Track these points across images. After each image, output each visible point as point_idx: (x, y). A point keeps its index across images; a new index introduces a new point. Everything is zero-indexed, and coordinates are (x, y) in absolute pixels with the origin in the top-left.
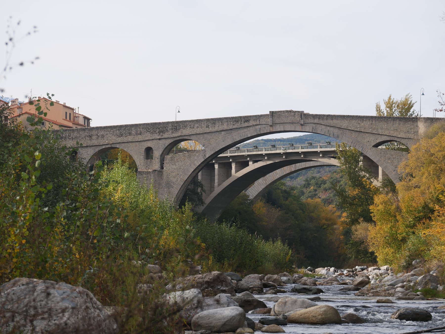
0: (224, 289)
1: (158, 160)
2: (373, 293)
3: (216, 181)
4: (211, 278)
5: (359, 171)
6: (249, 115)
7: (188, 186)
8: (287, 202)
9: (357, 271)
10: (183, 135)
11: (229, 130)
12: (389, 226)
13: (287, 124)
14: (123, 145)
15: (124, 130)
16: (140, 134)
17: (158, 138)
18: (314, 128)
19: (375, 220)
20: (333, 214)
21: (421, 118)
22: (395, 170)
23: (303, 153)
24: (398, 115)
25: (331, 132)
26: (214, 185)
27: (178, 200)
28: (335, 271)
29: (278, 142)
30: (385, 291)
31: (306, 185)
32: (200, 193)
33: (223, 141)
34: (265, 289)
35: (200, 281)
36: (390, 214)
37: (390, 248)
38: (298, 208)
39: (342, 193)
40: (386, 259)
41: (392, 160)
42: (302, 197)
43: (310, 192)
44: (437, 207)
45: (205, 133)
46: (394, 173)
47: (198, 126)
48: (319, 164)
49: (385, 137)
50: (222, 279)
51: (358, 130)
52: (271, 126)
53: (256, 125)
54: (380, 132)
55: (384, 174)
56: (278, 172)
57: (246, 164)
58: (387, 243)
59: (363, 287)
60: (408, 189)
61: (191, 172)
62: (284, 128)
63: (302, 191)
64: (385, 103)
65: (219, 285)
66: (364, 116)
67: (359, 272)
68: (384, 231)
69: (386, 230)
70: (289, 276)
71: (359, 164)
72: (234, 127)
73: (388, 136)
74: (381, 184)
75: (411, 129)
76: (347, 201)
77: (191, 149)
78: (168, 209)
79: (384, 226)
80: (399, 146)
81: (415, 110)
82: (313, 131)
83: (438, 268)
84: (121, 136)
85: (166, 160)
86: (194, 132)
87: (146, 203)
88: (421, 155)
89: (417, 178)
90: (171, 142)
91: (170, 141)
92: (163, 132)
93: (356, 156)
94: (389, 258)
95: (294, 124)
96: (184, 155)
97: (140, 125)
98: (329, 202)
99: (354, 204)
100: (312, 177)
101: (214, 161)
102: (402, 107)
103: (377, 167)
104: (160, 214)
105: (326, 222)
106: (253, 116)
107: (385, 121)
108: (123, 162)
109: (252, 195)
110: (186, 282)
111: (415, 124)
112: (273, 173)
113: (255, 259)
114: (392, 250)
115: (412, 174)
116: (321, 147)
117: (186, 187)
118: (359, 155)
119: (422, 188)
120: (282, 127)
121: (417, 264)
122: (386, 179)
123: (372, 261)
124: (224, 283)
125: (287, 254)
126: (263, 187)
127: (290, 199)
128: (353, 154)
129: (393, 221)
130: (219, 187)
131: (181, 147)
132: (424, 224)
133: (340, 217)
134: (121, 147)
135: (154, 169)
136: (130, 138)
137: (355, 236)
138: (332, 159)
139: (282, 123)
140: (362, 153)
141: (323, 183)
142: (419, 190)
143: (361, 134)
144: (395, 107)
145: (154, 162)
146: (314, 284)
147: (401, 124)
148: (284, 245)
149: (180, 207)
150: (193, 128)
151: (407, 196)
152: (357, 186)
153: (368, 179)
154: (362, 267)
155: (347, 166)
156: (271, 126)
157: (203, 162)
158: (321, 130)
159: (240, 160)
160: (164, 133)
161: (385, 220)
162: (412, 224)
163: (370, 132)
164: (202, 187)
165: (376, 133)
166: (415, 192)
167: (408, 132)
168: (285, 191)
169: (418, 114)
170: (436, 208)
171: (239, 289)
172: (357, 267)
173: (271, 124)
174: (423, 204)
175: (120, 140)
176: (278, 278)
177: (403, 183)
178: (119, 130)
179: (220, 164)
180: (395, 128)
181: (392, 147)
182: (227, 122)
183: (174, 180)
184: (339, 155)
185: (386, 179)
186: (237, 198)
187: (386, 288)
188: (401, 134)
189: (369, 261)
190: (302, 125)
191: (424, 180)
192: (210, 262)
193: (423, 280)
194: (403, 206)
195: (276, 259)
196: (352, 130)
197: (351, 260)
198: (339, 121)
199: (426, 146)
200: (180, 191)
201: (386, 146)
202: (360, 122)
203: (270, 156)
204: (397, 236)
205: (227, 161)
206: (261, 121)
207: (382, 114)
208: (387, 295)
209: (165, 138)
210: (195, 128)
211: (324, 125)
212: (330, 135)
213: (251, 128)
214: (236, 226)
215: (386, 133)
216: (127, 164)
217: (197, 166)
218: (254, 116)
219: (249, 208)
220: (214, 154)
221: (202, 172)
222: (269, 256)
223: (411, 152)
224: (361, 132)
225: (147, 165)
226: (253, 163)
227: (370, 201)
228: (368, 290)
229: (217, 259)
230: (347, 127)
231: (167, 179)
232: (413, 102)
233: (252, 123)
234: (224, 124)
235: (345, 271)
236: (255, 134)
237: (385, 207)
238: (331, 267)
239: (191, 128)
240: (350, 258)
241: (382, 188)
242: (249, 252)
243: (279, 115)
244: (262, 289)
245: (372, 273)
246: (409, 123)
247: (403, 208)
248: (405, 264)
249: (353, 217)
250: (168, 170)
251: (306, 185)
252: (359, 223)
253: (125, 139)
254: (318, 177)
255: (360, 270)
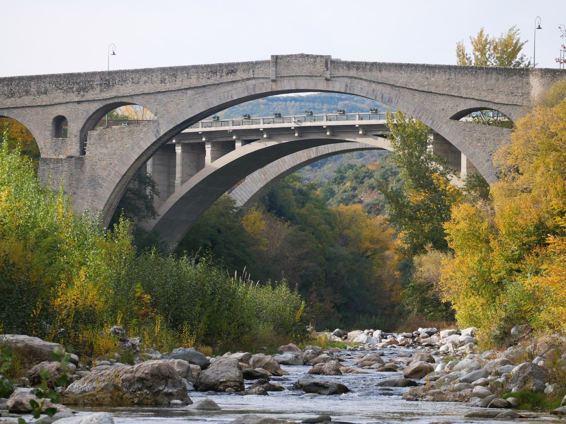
0: (170, 391)
1: (76, 138)
2: (433, 394)
3: (178, 175)
4: (146, 372)
5: (426, 161)
6: (235, 62)
7: (128, 184)
8: (303, 211)
9: (421, 336)
10: (119, 95)
11: (201, 87)
12: (477, 259)
13: (301, 78)
14: (15, 111)
15: (17, 85)
16: (45, 93)
17: (77, 100)
18: (349, 85)
19: (452, 247)
20: (384, 231)
21: (536, 70)
22: (488, 160)
23: (329, 127)
24: (495, 64)
25: (379, 93)
26: (174, 183)
27: (111, 209)
28: (383, 337)
29: (291, 101)
30: (454, 391)
31: (338, 179)
32: (150, 197)
33: (190, 107)
34: (249, 381)
35: (128, 378)
36: (478, 237)
37: (477, 297)
38: (321, 220)
39: (397, 198)
40: (470, 316)
41: (485, 141)
42: (330, 201)
43: (345, 191)
44: (551, 239)
45: (159, 92)
46: (487, 164)
47: (147, 79)
48: (358, 146)
49: (473, 101)
50: (167, 375)
51: (426, 89)
52: (274, 81)
53: (248, 79)
54: (464, 93)
55: (470, 166)
56: (287, 160)
57: (230, 146)
58: (472, 287)
59: (421, 378)
60: (511, 193)
61: (134, 160)
62: (296, 84)
63: (331, 189)
64: (472, 43)
65: (162, 384)
66: (436, 65)
67: (424, 338)
68: (468, 267)
69: (471, 264)
70: (297, 350)
71: (427, 148)
72: (209, 82)
73: (477, 100)
74: (465, 183)
75: (517, 88)
76: (405, 212)
77: (136, 118)
78: (88, 230)
79: (469, 259)
80: (496, 118)
81: (525, 56)
82: (346, 90)
83: (549, 349)
84: (12, 97)
85: (90, 139)
86: (140, 90)
87: (49, 220)
88: (533, 136)
89: (526, 175)
90: (98, 108)
91: (98, 106)
92: (85, 89)
93: (422, 135)
94: (476, 314)
95: (314, 78)
96: (122, 130)
97: (45, 77)
98: (378, 209)
99: (417, 219)
100: (349, 164)
101: (174, 141)
102: (502, 50)
103: (458, 154)
104: (74, 238)
105: (372, 246)
106: (243, 64)
107: (472, 74)
108: (11, 147)
109: (240, 199)
110: (104, 378)
111: (525, 80)
112: (279, 162)
113: (237, 321)
114: (482, 301)
115: (517, 168)
116: (361, 118)
117: (124, 187)
118: (426, 133)
119: (535, 193)
120: (292, 82)
121: (520, 332)
122: (473, 176)
123: (446, 317)
124: (170, 380)
125: (297, 308)
126: (261, 185)
127: (309, 205)
128: (417, 130)
129: (483, 249)
130: (183, 186)
131: (118, 114)
132: (537, 255)
133: (395, 236)
134: (13, 114)
135: (69, 154)
136: (27, 100)
137: (418, 274)
138: (380, 138)
139: (293, 76)
140: (432, 129)
141: (368, 176)
142: (529, 197)
143: (431, 97)
144: (489, 50)
145: (69, 142)
146: (336, 370)
147: (500, 79)
148: (292, 291)
149: (111, 227)
150: (138, 83)
151: (508, 207)
152: (422, 186)
153: (442, 174)
154: (429, 329)
155: (406, 151)
156: (274, 81)
157: (155, 143)
158: (362, 89)
159: (220, 140)
160: (87, 92)
161: (470, 248)
162: (516, 255)
163: (446, 93)
164: (153, 187)
165: (456, 94)
166: (522, 201)
167: (512, 93)
168: (300, 191)
169: (529, 63)
170: (549, 240)
171: (201, 383)
172: (420, 330)
173: (274, 77)
174: (535, 221)
175: (9, 102)
176: (272, 361)
177: (501, 183)
178: (8, 85)
179: (184, 146)
180: (490, 87)
181: (485, 119)
182: (197, 73)
183: (104, 174)
184: (392, 133)
185: (473, 176)
186: (215, 204)
187: (456, 385)
188: (500, 97)
189: (443, 317)
190: (327, 80)
191: (538, 179)
192: (157, 329)
193: (521, 374)
194: (500, 223)
195: (279, 317)
196: (415, 90)
197: (411, 315)
198: (392, 74)
199: (542, 119)
200: (114, 194)
201: (474, 117)
202: (428, 75)
203: (272, 133)
204: (490, 275)
205: (198, 141)
206: (256, 72)
207: (467, 61)
208: (457, 399)
209: (88, 101)
210: (141, 83)
211: (366, 80)
212: (376, 97)
213: (239, 85)
214: (206, 262)
215: (475, 95)
216: (18, 150)
217: (143, 150)
218: (244, 63)
219: (235, 222)
220: (174, 128)
221: (154, 160)
222: (266, 312)
223: (516, 131)
224: (431, 92)
225: (56, 147)
226: (242, 145)
227: (445, 213)
228: (424, 390)
229: (171, 322)
230: (406, 84)
231: (92, 172)
232: (521, 42)
233: (240, 75)
234: (192, 77)
235: (400, 335)
236: (246, 95)
237: (470, 225)
238: (375, 330)
239: (133, 83)
240: (409, 312)
241: (466, 191)
242: (228, 309)
243: (288, 62)
244: (242, 384)
245: (447, 340)
246: (514, 77)
247: (501, 227)
248: (498, 332)
249: (415, 241)
250: (94, 157)
251: (338, 179)
252: (426, 252)
253: (18, 102)
254: (359, 165)
255: (426, 335)
